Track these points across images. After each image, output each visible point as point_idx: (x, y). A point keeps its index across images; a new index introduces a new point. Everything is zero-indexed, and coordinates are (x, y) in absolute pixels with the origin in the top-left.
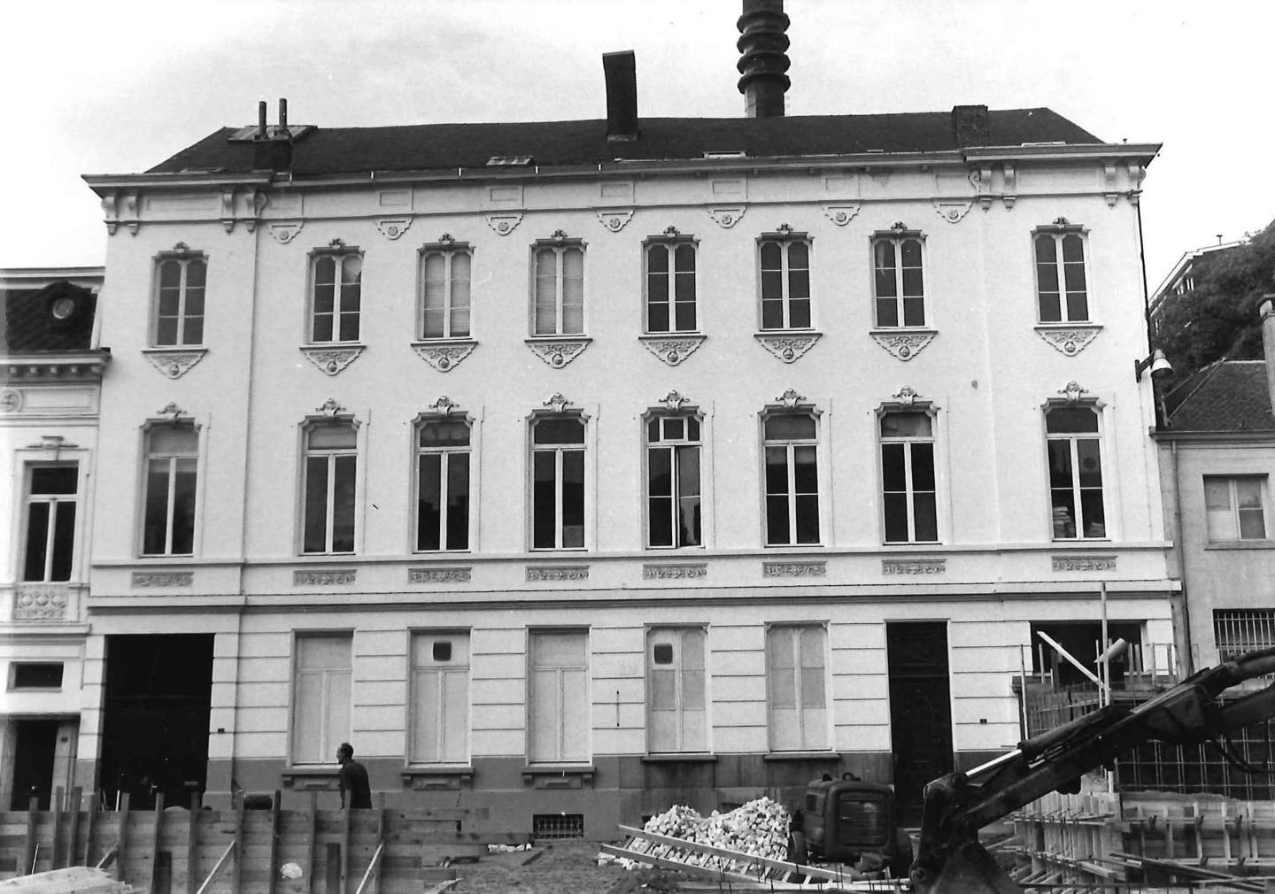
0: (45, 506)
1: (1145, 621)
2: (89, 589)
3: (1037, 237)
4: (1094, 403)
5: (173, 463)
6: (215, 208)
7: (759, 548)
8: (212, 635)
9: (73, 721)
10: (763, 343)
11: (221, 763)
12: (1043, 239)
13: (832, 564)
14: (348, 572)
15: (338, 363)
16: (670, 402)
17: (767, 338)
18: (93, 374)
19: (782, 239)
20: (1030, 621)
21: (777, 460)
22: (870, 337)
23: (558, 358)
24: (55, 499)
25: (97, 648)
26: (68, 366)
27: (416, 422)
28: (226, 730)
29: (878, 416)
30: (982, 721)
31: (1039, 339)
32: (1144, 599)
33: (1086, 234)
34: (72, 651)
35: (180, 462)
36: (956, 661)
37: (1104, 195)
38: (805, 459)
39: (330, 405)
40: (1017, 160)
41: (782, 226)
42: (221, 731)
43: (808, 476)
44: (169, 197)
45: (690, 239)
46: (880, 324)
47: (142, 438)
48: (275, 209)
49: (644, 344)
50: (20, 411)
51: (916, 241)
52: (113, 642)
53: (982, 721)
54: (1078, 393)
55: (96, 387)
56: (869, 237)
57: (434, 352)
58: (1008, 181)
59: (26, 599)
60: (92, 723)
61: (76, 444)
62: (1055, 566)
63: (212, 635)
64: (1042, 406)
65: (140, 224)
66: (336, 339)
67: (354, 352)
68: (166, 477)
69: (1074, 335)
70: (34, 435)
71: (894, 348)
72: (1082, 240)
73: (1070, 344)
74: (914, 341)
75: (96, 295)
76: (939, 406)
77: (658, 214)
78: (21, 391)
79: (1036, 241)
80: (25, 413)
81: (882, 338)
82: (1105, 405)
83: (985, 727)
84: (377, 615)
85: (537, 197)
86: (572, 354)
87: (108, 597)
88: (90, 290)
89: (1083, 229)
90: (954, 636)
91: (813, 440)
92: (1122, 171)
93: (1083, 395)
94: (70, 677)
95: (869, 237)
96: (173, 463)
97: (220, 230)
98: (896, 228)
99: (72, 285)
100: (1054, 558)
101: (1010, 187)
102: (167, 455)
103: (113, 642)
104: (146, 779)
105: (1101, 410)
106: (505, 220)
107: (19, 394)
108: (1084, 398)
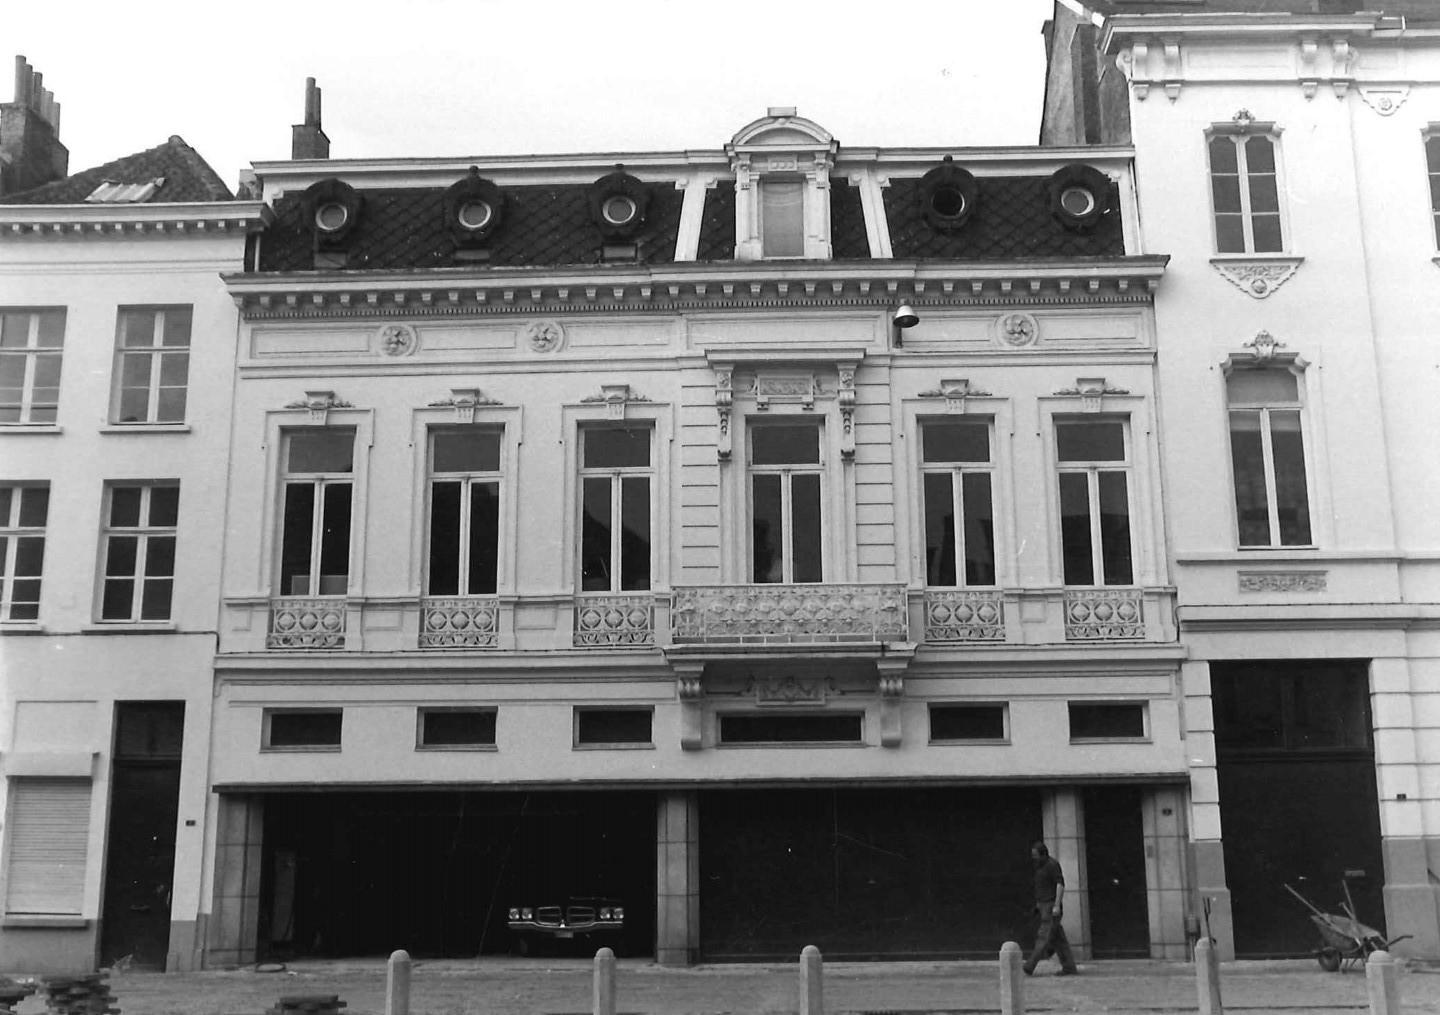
0: (308, 489)
1: (1371, 659)
2: (1174, 595)
3: (1212, 139)
4: (1291, 362)
5: (1265, 417)
6: (1286, 64)
7: (1232, 550)
8: (1368, 661)
9: (1178, 785)
10: (1223, 271)
11: (1405, 844)
12: (1220, 143)
13: (1335, 574)
14: (1317, 573)
15: (1267, 282)
16: (1259, 347)
17: (1226, 265)
18: (1142, 290)
19: (1238, 131)
20: (1209, 661)
21: (1245, 426)
22: (1212, 267)
23: (1259, 283)
24: (469, 478)
25: (1199, 680)
26: (283, 295)
27: (1225, 367)
28: (1408, 797)
29: (1224, 373)
30: (1399, 796)
31: (1216, 275)
32: (1278, 630)
33: (1278, 135)
34: (1162, 684)
35: (1274, 416)
36: (1384, 711)
37: (1300, 82)
38: (1285, 426)
39: (1262, 340)
40: (1181, 33)
41: (1241, 113)
42: (1402, 798)
43: (1290, 447)
44: (1217, 48)
45: (1268, 128)
46: (1220, 251)
47: (1225, 387)
48: (1364, 68)
49: (1218, 269)
50: (1035, 344)
51: (1265, 139)
52: (1224, 673)
53: (1399, 796)
54: (1271, 347)
55: (1145, 311)
56: (1204, 130)
57: (1243, 271)
58: (1169, 61)
59: (286, 620)
60: (1206, 785)
61: (1125, 389)
62: (1242, 584)
63: (1368, 661)
64: (1221, 365)
65: (1352, 84)
66: (1250, 252)
67: (1289, 267)
68: (1256, 437)
69: (1264, 269)
70: (294, 391)
71: (1245, 281)
72: (1272, 144)
73: (1260, 282)
74: (1272, 272)
75: (1117, 183)
76: (1308, 361)
77: (1227, 92)
78: (414, 327)
79: (1210, 145)
80: (1044, 346)
81: (1226, 269)
82: (1308, 364)
83: (1405, 805)
84: (1349, 635)
85: (1199, 66)
86: (1277, 278)
87: (1289, 605)
88: (846, 180)
89: (1275, 127)
90: (1380, 678)
91: (1294, 404)
92: (1156, 54)
93: (1279, 350)
94: (1158, 721)
95: (1204, 130)
96: (1265, 417)
97: (1296, 95)
98: (1240, 118)
99: (484, 180)
100: (1240, 573)
101: (1174, 69)
102: (1254, 405)
103: (1224, 673)
104: (162, 887)
105: (1302, 371)
106: (1386, 96)
107: (410, 330)
108: (1278, 354)
